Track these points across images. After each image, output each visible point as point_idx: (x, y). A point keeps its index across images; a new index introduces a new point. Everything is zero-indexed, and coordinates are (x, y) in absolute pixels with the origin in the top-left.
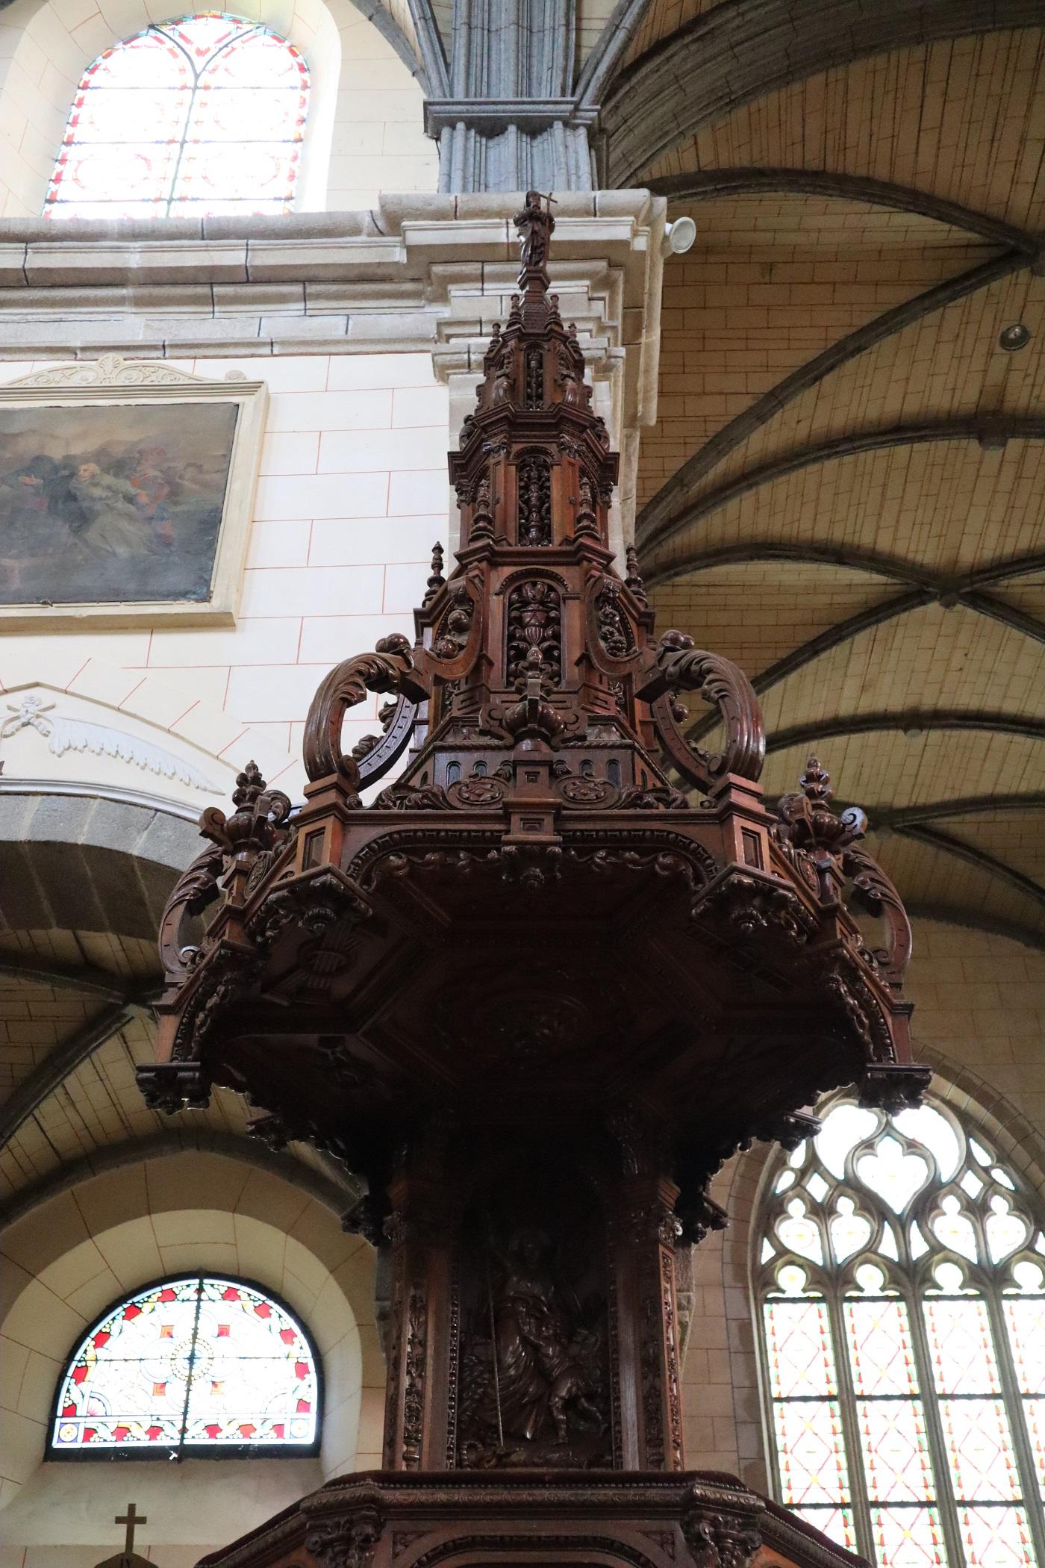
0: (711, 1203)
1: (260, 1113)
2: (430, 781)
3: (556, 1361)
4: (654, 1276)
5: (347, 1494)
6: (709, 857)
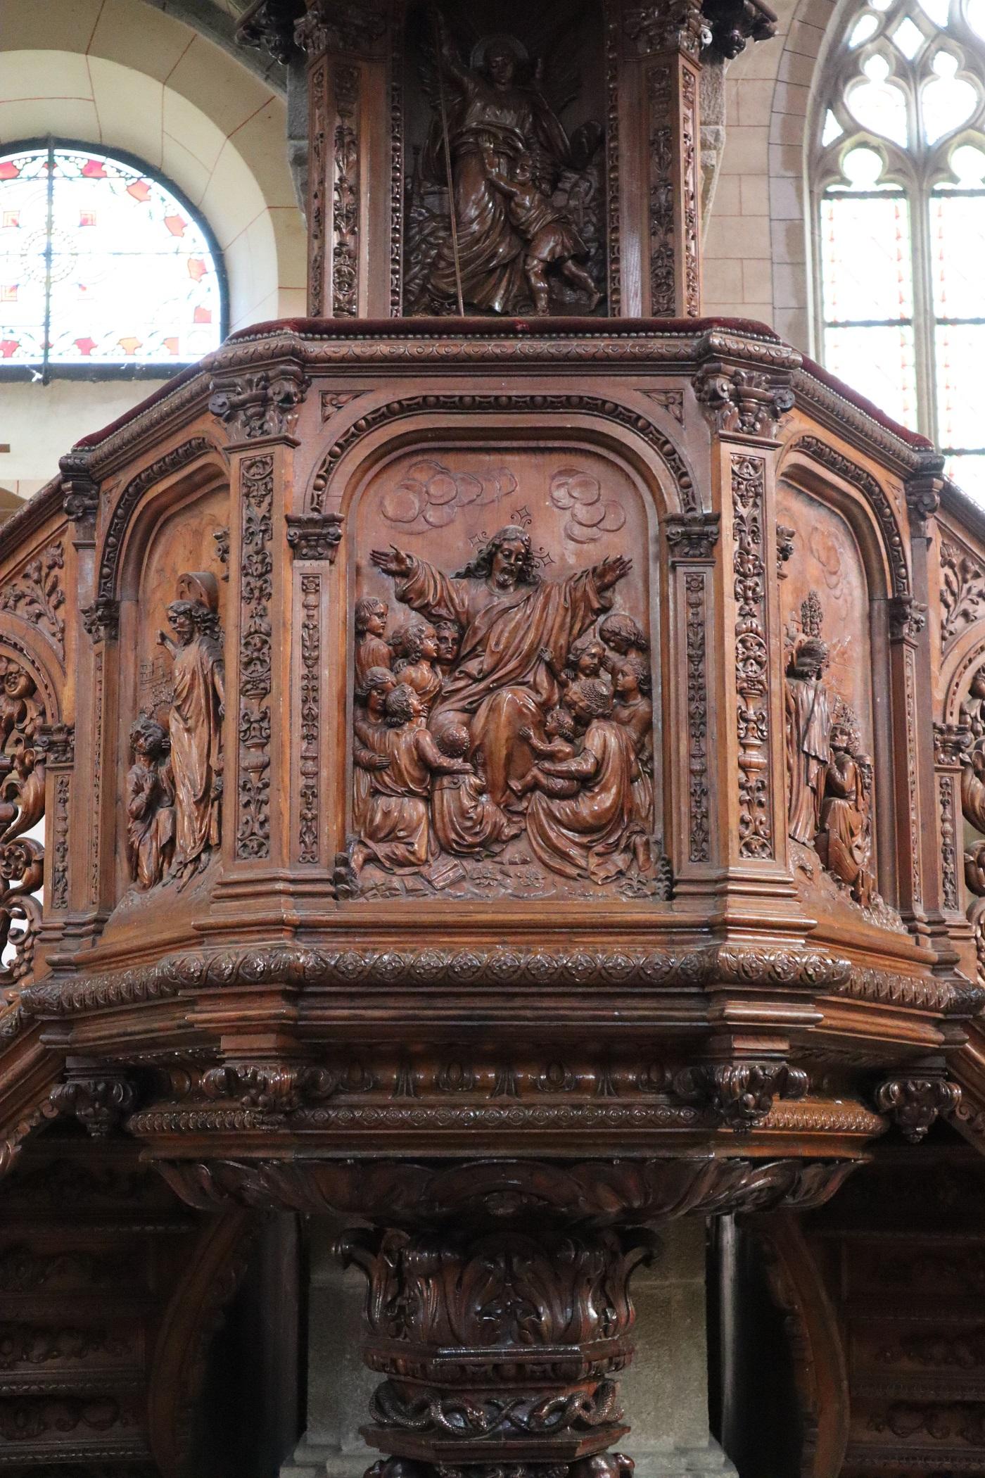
3: (534, 213)
4: (670, 97)
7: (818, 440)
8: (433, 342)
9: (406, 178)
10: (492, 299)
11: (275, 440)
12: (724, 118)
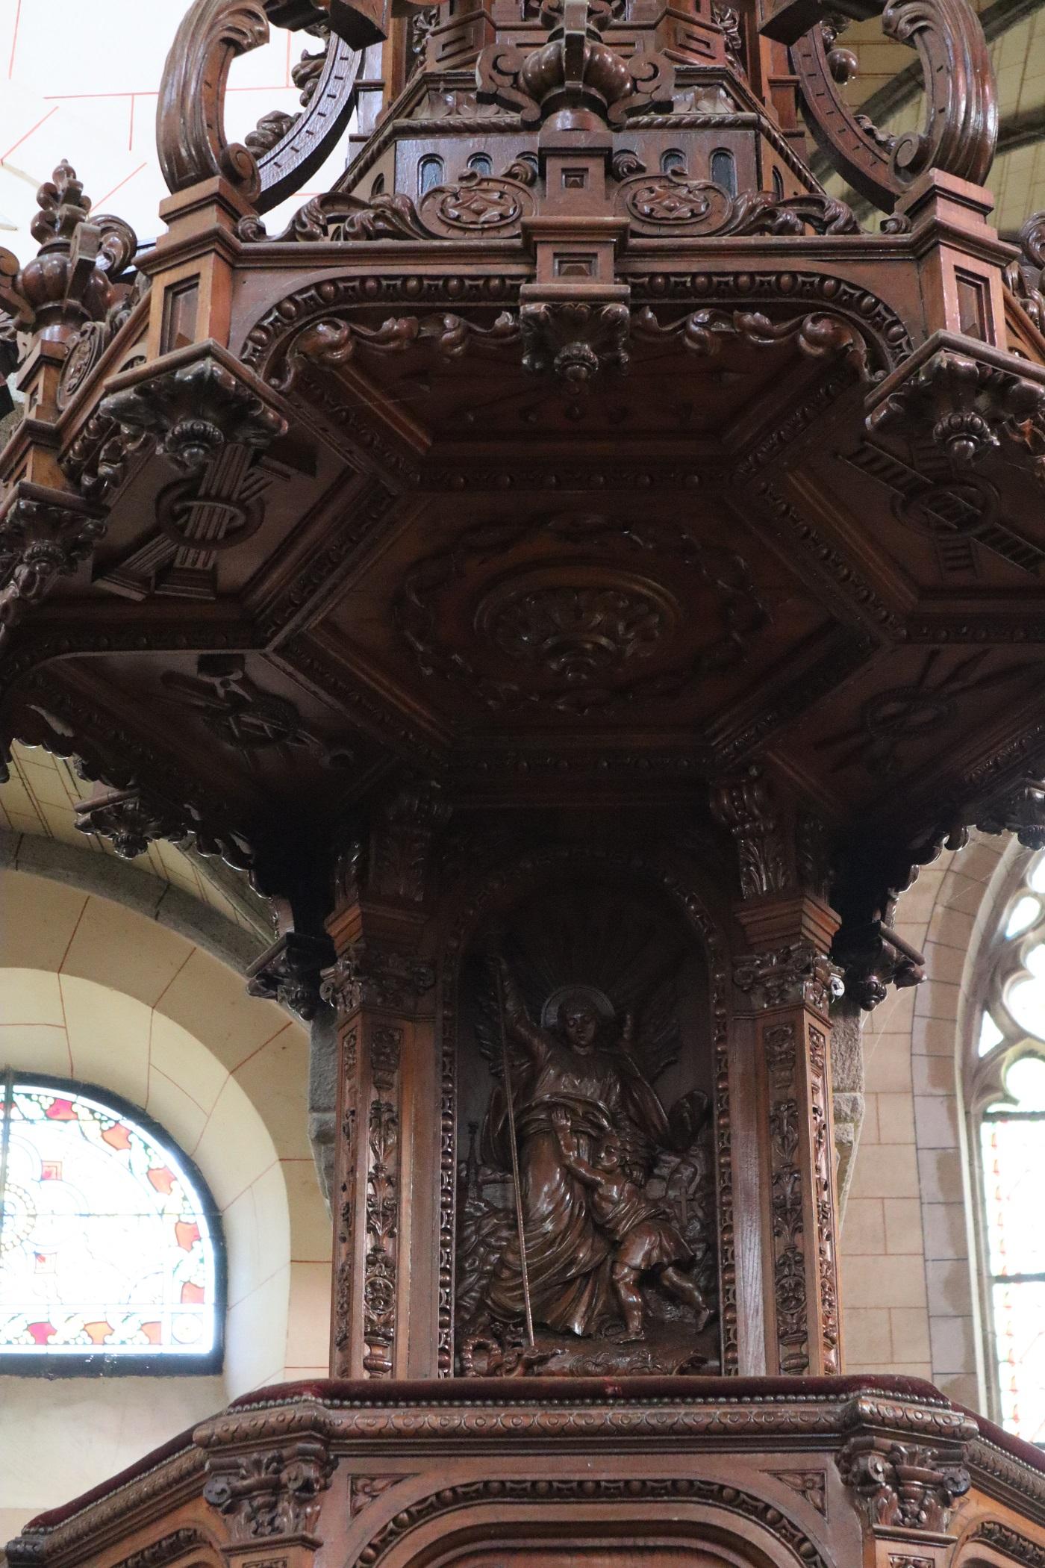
0: (893, 941)
1: (96, 791)
2: (388, 187)
4: (794, 1062)
5: (271, 1416)
6: (897, 322)
7: (1001, 1526)
8: (497, 1410)
9: (459, 1163)
10: (570, 1317)
11: (290, 1540)
12: (863, 1083)
